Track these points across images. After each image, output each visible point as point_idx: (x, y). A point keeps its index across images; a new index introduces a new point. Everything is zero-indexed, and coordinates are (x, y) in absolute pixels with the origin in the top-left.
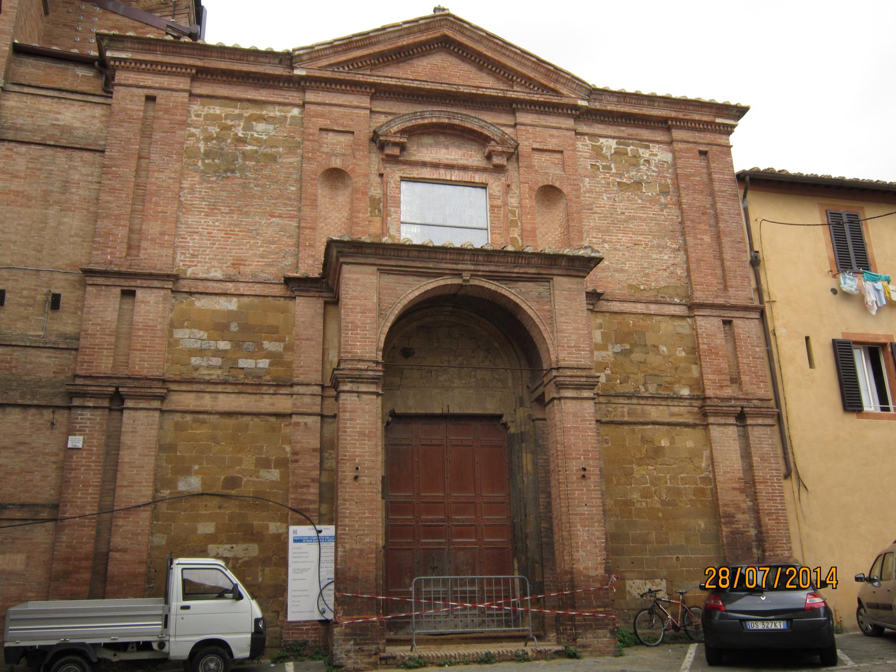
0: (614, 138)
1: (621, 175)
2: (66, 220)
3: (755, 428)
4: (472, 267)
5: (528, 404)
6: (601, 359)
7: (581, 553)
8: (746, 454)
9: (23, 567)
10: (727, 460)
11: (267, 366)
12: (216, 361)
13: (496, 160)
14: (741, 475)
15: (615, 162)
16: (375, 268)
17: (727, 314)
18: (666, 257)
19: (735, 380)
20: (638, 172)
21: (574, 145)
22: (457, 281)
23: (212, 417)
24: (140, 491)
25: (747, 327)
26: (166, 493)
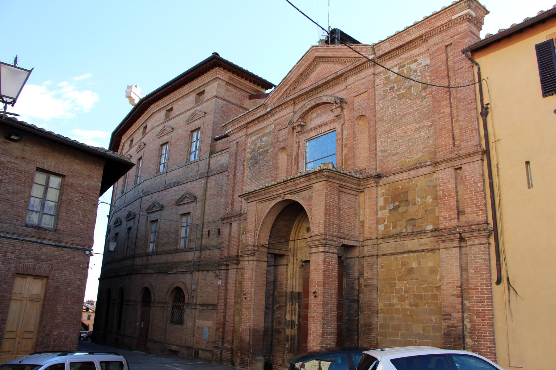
7: (312, 338)
8: (463, 269)
10: (450, 273)
16: (255, 202)
17: (457, 163)
18: (423, 134)
25: (473, 169)
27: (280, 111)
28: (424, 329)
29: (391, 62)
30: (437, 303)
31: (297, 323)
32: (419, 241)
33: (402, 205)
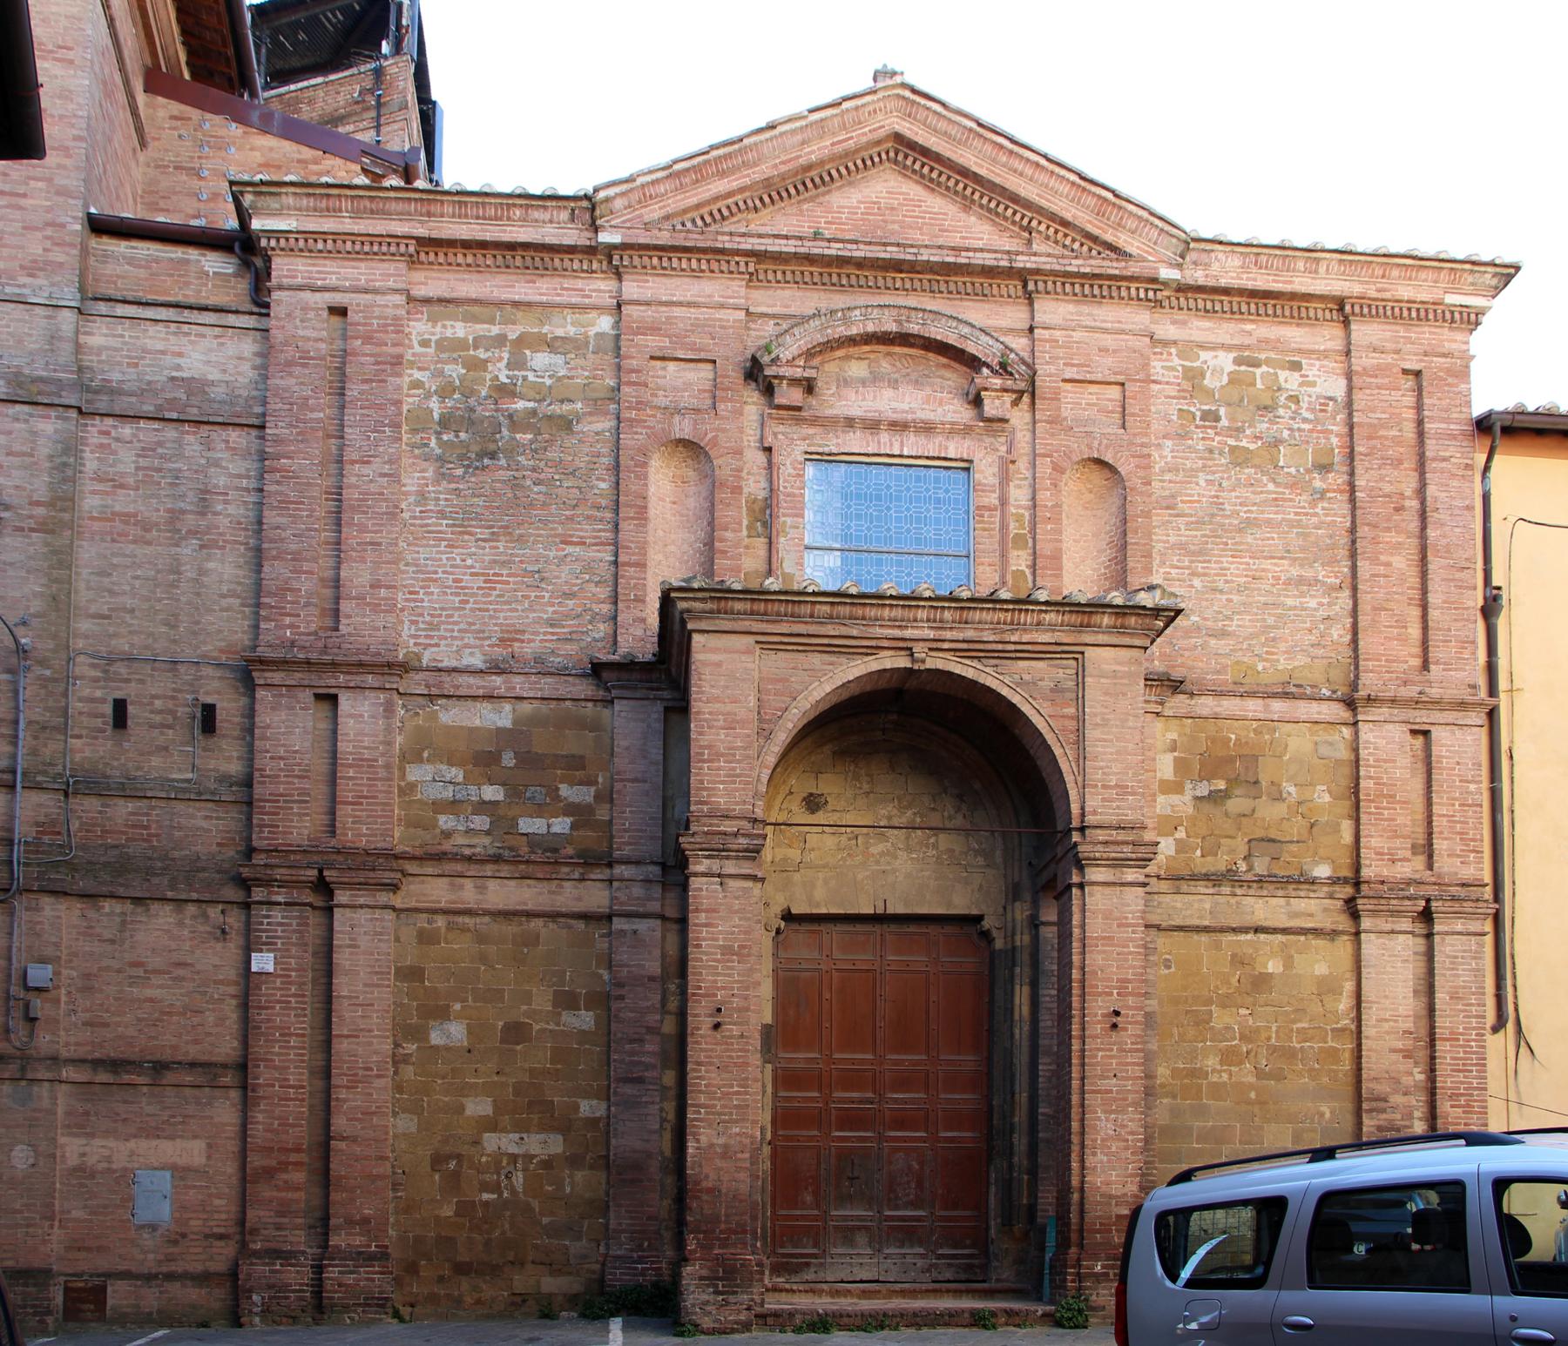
2: (211, 565)
4: (931, 634)
5: (1027, 896)
7: (1100, 1157)
9: (204, 1160)
12: (481, 822)
14: (1409, 1025)
16: (751, 639)
18: (1313, 604)
22: (902, 662)
24: (370, 1044)
26: (410, 1048)
27: (665, 272)
29: (1207, 324)
30: (1335, 1071)
32: (1288, 904)
33: (1237, 792)
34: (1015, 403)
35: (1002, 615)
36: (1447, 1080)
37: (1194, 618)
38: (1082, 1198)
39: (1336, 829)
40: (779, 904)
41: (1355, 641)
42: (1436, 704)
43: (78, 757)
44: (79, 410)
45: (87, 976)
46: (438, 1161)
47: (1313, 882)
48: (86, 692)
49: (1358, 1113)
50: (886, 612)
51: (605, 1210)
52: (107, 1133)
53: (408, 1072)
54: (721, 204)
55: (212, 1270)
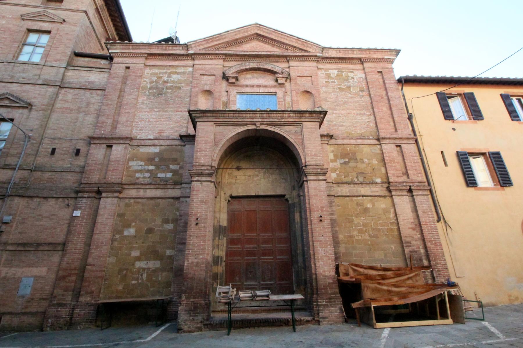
0: (336, 69)
1: (340, 85)
2: (87, 118)
3: (418, 196)
4: (261, 120)
5: (297, 189)
6: (333, 167)
7: (321, 263)
8: (415, 210)
9: (45, 274)
11: (171, 176)
12: (147, 175)
13: (280, 81)
14: (412, 221)
15: (337, 79)
16: (213, 123)
19: (407, 174)
20: (348, 82)
21: (317, 73)
22: (254, 127)
23: (143, 200)
24: (104, 236)
26: (117, 236)
27: (204, 59)
28: (385, 256)
31: (224, 259)
34: (286, 81)
35: (279, 115)
36: (427, 237)
37: (334, 123)
38: (316, 277)
39: (381, 170)
40: (229, 193)
41: (377, 126)
42: (401, 139)
43: (38, 162)
44: (60, 86)
45: (24, 219)
46: (120, 271)
47: (376, 183)
48: (45, 147)
49: (403, 247)
50: (248, 115)
51: (170, 286)
52: (17, 266)
53: (116, 244)
54: (218, 46)
55: (39, 311)
